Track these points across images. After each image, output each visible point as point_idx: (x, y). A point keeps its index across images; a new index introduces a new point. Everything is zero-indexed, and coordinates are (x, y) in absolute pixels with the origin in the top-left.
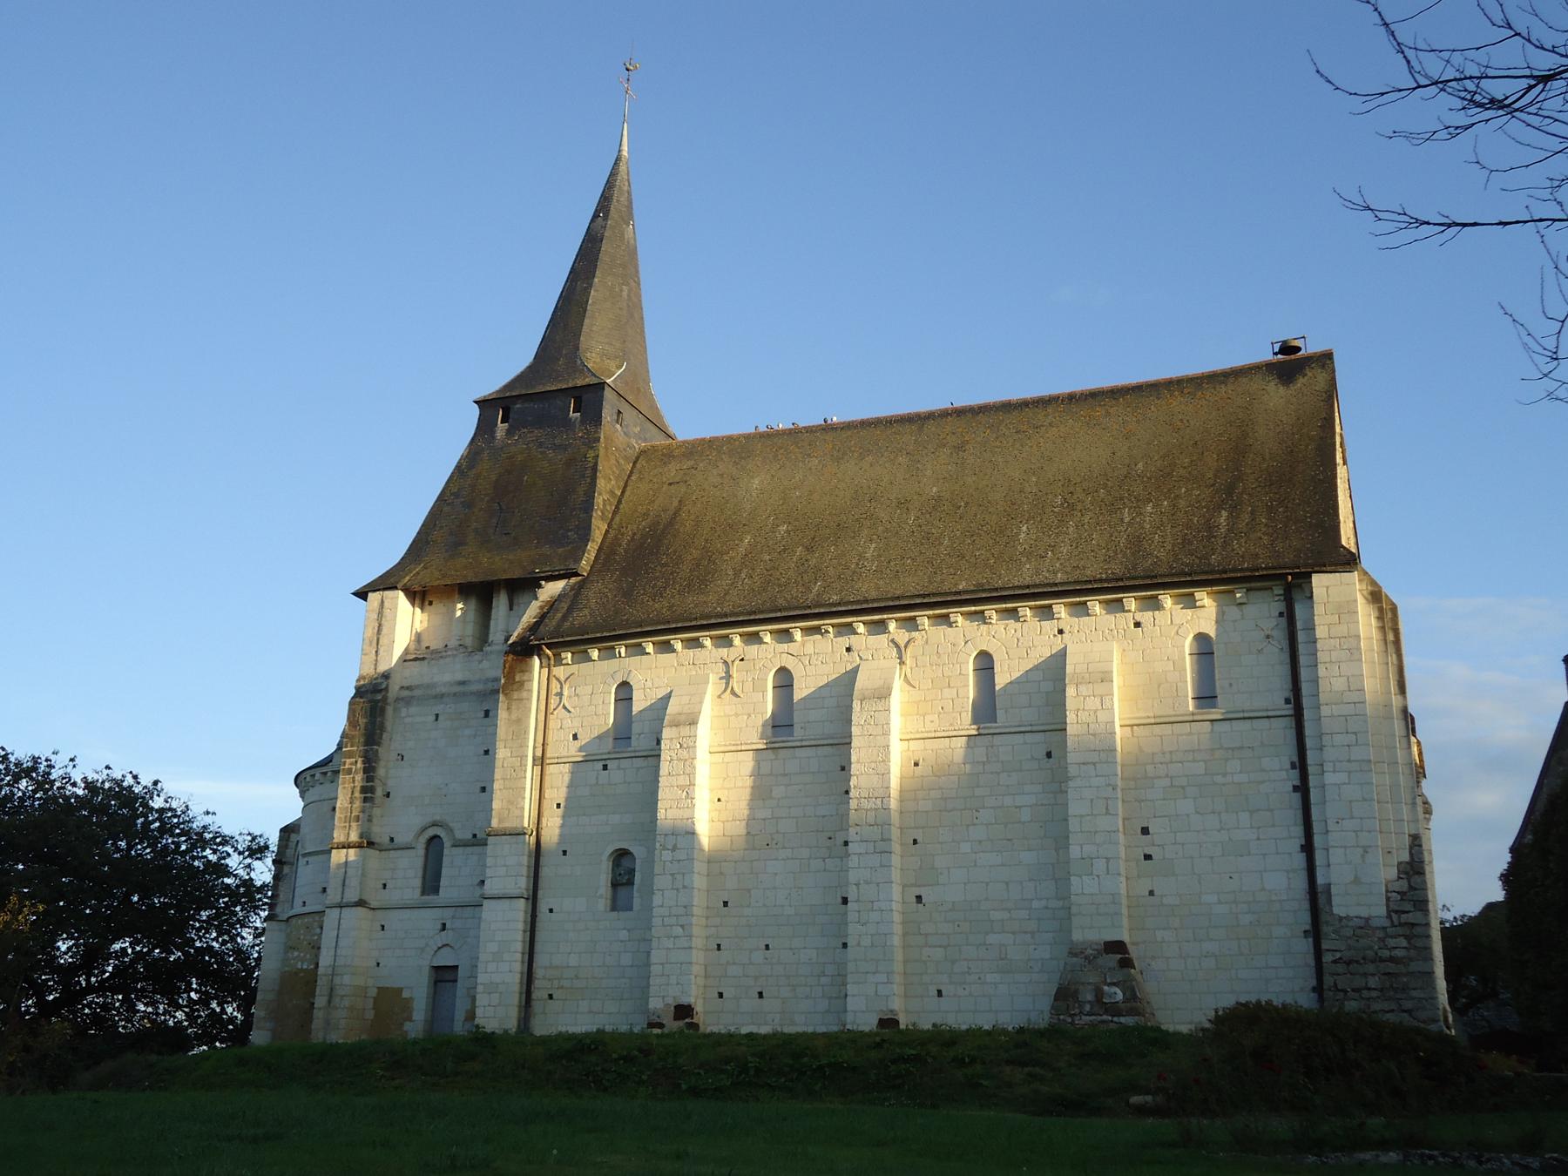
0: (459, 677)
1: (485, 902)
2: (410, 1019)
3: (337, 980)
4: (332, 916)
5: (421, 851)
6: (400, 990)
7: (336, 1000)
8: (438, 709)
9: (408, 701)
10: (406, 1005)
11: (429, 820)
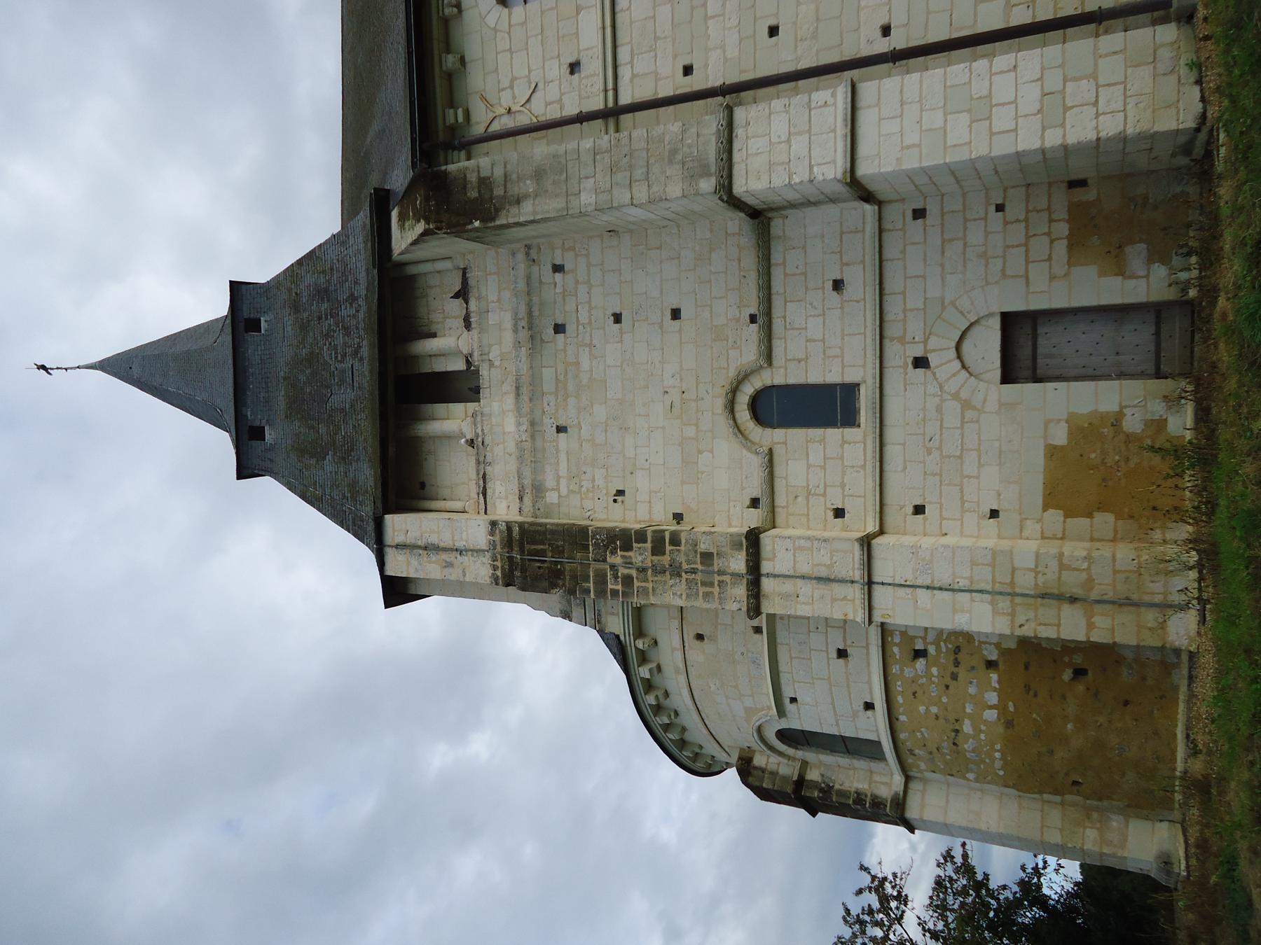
0: (510, 401)
1: (878, 618)
2: (1116, 420)
3: (1025, 582)
4: (897, 609)
5: (779, 434)
6: (1052, 452)
7: (1072, 583)
8: (549, 426)
9: (539, 490)
10: (1087, 432)
11: (723, 422)
